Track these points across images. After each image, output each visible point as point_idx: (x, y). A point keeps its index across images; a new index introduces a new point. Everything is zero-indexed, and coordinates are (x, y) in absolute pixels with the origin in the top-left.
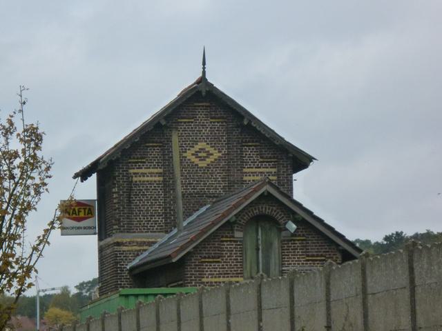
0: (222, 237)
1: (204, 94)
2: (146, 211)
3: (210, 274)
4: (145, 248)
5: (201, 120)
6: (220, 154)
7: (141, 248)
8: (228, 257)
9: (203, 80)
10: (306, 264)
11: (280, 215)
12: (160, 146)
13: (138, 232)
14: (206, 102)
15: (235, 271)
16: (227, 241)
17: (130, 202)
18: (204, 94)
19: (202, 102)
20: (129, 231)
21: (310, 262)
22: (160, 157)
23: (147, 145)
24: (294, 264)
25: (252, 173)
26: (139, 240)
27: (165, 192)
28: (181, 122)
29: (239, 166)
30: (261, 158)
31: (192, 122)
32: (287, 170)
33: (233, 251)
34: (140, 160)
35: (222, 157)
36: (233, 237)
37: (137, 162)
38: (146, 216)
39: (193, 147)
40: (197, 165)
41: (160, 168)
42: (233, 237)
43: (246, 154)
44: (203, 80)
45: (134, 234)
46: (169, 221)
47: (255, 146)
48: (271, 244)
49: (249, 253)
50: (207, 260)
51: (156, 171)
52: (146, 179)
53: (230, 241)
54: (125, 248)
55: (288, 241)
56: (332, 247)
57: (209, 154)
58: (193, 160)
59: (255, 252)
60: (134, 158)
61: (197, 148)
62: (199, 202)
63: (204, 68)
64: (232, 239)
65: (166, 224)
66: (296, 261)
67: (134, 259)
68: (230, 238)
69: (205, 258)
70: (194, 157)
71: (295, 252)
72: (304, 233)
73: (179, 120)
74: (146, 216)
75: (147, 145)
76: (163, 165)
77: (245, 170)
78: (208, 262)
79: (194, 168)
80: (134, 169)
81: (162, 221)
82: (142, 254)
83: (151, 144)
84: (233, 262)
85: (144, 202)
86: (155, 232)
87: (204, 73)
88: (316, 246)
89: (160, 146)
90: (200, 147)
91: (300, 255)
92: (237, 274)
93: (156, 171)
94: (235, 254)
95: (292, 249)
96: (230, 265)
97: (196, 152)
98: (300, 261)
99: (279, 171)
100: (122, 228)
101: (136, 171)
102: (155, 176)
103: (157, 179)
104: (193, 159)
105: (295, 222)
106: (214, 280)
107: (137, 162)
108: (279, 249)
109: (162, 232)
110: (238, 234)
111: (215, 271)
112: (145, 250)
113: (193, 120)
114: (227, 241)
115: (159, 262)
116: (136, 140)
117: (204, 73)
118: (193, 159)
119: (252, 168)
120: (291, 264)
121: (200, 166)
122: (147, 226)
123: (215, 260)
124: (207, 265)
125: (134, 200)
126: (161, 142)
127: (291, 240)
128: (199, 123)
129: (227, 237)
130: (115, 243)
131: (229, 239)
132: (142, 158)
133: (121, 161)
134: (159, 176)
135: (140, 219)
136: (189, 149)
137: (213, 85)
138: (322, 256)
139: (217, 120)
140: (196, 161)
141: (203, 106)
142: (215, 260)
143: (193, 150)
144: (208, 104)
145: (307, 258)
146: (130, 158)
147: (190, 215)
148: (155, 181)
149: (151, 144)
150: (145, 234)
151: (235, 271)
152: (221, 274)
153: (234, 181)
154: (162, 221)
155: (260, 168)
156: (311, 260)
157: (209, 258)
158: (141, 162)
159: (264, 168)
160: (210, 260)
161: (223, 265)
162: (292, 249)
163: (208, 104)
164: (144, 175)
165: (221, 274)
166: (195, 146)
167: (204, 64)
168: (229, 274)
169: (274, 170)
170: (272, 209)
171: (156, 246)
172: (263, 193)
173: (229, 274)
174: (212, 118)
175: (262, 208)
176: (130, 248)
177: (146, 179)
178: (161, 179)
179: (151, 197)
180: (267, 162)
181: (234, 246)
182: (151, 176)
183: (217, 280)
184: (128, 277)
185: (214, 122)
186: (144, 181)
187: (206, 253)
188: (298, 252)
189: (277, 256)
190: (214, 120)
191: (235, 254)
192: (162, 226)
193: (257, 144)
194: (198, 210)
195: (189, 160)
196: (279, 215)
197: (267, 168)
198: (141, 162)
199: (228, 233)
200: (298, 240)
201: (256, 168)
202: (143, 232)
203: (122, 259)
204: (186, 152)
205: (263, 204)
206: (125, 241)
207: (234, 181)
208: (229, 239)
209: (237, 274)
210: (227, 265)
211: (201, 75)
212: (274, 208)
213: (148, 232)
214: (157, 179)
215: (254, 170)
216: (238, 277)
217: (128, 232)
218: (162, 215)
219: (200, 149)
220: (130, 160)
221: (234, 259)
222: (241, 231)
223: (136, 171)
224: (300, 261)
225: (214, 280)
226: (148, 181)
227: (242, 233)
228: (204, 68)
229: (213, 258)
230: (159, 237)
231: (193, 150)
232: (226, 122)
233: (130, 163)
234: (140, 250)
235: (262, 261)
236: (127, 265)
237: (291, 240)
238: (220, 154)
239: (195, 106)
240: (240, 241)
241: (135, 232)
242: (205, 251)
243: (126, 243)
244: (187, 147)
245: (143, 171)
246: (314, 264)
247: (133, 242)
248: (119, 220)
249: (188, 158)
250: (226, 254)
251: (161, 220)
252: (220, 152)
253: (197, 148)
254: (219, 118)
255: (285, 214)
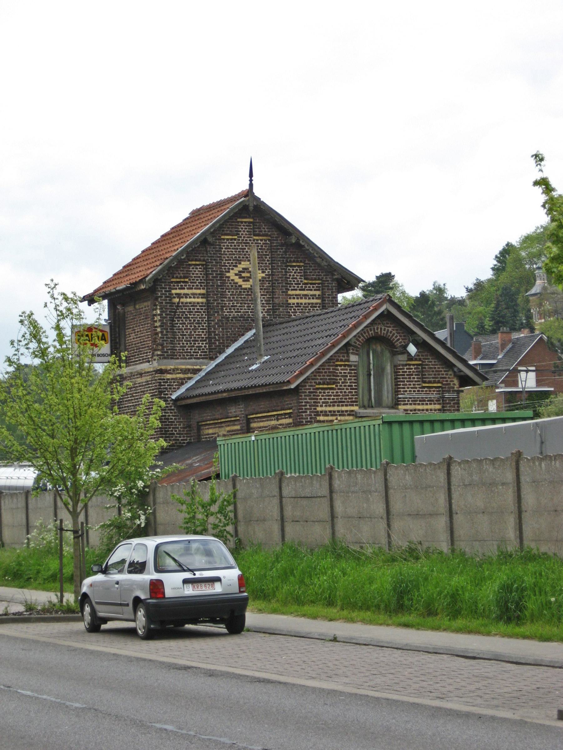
0: (337, 361)
1: (251, 208)
2: (189, 335)
3: (323, 403)
4: (190, 375)
5: (244, 237)
6: (264, 275)
7: (186, 376)
8: (342, 383)
9: (249, 193)
10: (422, 391)
11: (396, 337)
12: (202, 265)
13: (181, 359)
14: (249, 218)
15: (349, 398)
16: (341, 366)
17: (173, 326)
18: (251, 208)
19: (246, 218)
20: (173, 356)
21: (426, 389)
22: (203, 277)
23: (190, 263)
24: (410, 391)
25: (296, 295)
26: (183, 367)
27: (209, 315)
28: (224, 239)
29: (284, 288)
30: (305, 279)
31: (235, 239)
32: (332, 292)
33: (347, 376)
34: (182, 280)
35: (266, 278)
36: (348, 361)
37: (180, 282)
38: (190, 341)
39: (236, 266)
40: (240, 286)
41: (203, 289)
42: (348, 361)
43: (290, 275)
44: (249, 193)
45: (177, 361)
46: (213, 347)
47: (299, 266)
48: (383, 369)
49: (361, 378)
50: (321, 386)
51: (198, 291)
52: (189, 300)
53: (345, 365)
54: (169, 376)
55: (403, 365)
56: (449, 373)
57: (239, 275)
58: (236, 281)
59: (366, 377)
60: (177, 278)
61: (240, 267)
62: (245, 326)
63: (251, 180)
64: (346, 363)
65: (210, 350)
66: (412, 388)
67: (178, 388)
68: (345, 361)
69: (320, 384)
70: (237, 277)
71: (410, 378)
72: (421, 357)
73: (223, 237)
74: (190, 341)
75: (190, 263)
76: (207, 286)
77: (290, 292)
78: (322, 389)
79: (238, 289)
80: (176, 289)
81: (205, 347)
82: (186, 382)
83: (194, 263)
84: (347, 389)
85: (187, 326)
86: (199, 358)
87: (251, 185)
88: (433, 371)
89: (202, 265)
90: (244, 267)
91: (416, 381)
92: (351, 402)
93: (198, 291)
94: (349, 379)
95: (407, 375)
96: (345, 392)
97: (240, 272)
98: (416, 388)
99: (323, 294)
100: (166, 354)
101: (178, 291)
102: (198, 298)
103: (200, 300)
104: (237, 279)
105: (416, 345)
106: (328, 409)
107: (180, 282)
108: (391, 374)
109: (206, 358)
110: (353, 358)
111: (329, 399)
112: (190, 379)
113: (236, 237)
114: (341, 366)
115: (385, 393)
116: (182, 258)
117: (251, 185)
118: (237, 279)
119: (296, 290)
120: (406, 391)
121: (243, 286)
122: (190, 352)
123: (329, 386)
124: (320, 393)
125: (177, 324)
126: (204, 260)
127: (406, 365)
128: (243, 240)
129: (342, 361)
130: (158, 370)
131: (343, 363)
132: (185, 277)
133: (163, 280)
134: (202, 298)
135: (183, 344)
136: (232, 269)
137: (260, 199)
138: (439, 382)
139: (261, 238)
140: (240, 281)
141: (245, 222)
142: (329, 386)
143: (236, 270)
144: (251, 220)
145: (424, 385)
146: (173, 278)
147: (236, 341)
148: (198, 303)
149: (194, 263)
150: (188, 361)
151: (349, 398)
152: (336, 402)
153: (279, 304)
154: (205, 347)
155: (304, 290)
156: (427, 387)
157: (324, 384)
158: (184, 282)
159: (307, 290)
160: (325, 386)
161: (337, 392)
162: (407, 375)
163: (251, 220)
164: (186, 296)
165: (336, 402)
166: (239, 266)
167: (251, 175)
168: (344, 402)
169: (317, 293)
170: (388, 330)
171: (203, 374)
172: (384, 311)
173: (344, 402)
174: (255, 235)
175: (377, 329)
176: (174, 376)
177: (189, 300)
178: (204, 300)
179: (194, 321)
180: (311, 284)
181: (348, 371)
182: (194, 298)
183: (331, 409)
184: (173, 408)
185: (257, 240)
186: (186, 303)
187: (321, 379)
188: (414, 378)
189: (389, 382)
190: (257, 238)
191: (349, 379)
192: (206, 352)
193: (302, 264)
194: (243, 335)
195: (233, 280)
196: (397, 338)
197: (311, 290)
198: (184, 282)
199: (344, 356)
200: (414, 365)
201: (300, 290)
202: (186, 359)
203: (166, 388)
204: (229, 272)
205: (379, 324)
206: (169, 368)
207: (279, 304)
208: (343, 363)
209: (351, 402)
210: (341, 392)
211: (247, 187)
212: (390, 329)
213: (191, 358)
214: (200, 300)
215: (298, 292)
216: (353, 405)
217: (172, 358)
218: (205, 341)
219: (243, 269)
220: (173, 280)
221: (349, 386)
222: (357, 354)
223: (178, 291)
224: (416, 388)
225: (328, 409)
226: (190, 303)
227: (357, 357)
228: (251, 180)
229: (328, 384)
230: (206, 365)
231: (236, 270)
232: (269, 240)
233: (172, 282)
234: (184, 379)
235: (374, 389)
236: (171, 394)
237: (406, 365)
238: (264, 275)
239: (238, 222)
240: (355, 366)
241: (178, 358)
242: (320, 376)
243: (170, 370)
244: (230, 266)
245: (186, 291)
246: (430, 391)
247: (177, 369)
248: (162, 345)
249: (231, 278)
250: (340, 379)
251: (204, 345)
252: (263, 272)
253: (240, 267)
254: (263, 235)
255: (400, 336)
